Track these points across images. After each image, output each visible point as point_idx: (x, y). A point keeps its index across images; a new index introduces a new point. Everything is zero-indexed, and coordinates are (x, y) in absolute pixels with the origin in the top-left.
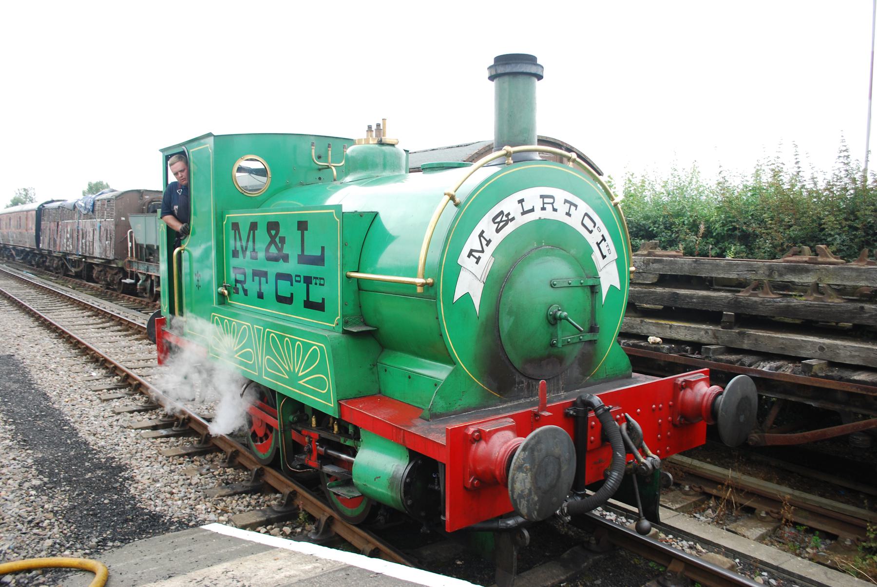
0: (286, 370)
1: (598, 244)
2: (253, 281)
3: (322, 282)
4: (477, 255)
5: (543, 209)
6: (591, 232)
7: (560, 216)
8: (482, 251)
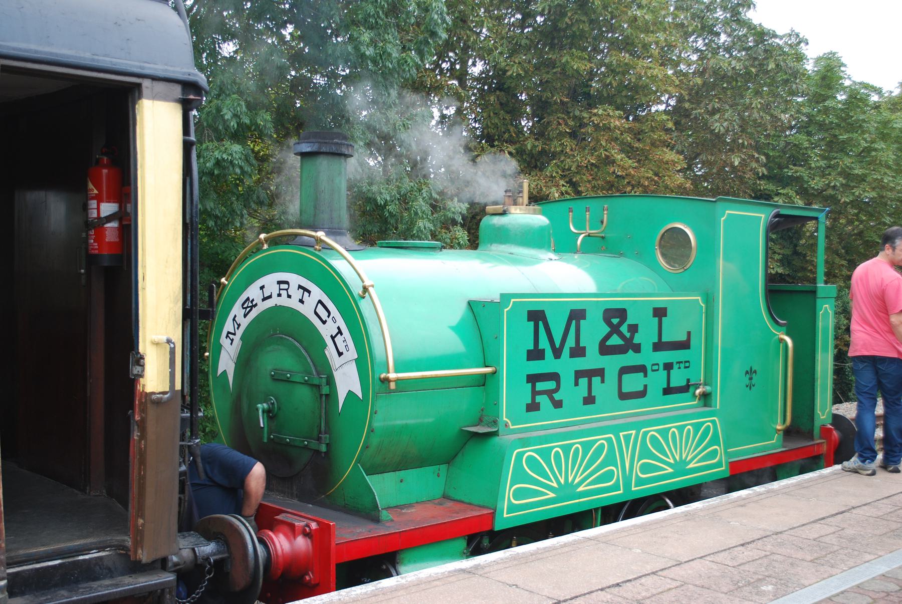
2: (576, 384)
3: (687, 364)
5: (279, 295)
7: (293, 304)
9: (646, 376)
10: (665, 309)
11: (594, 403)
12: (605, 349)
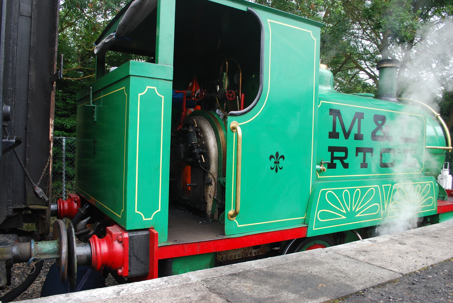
2: (357, 155)
10: (362, 114)
11: (335, 168)
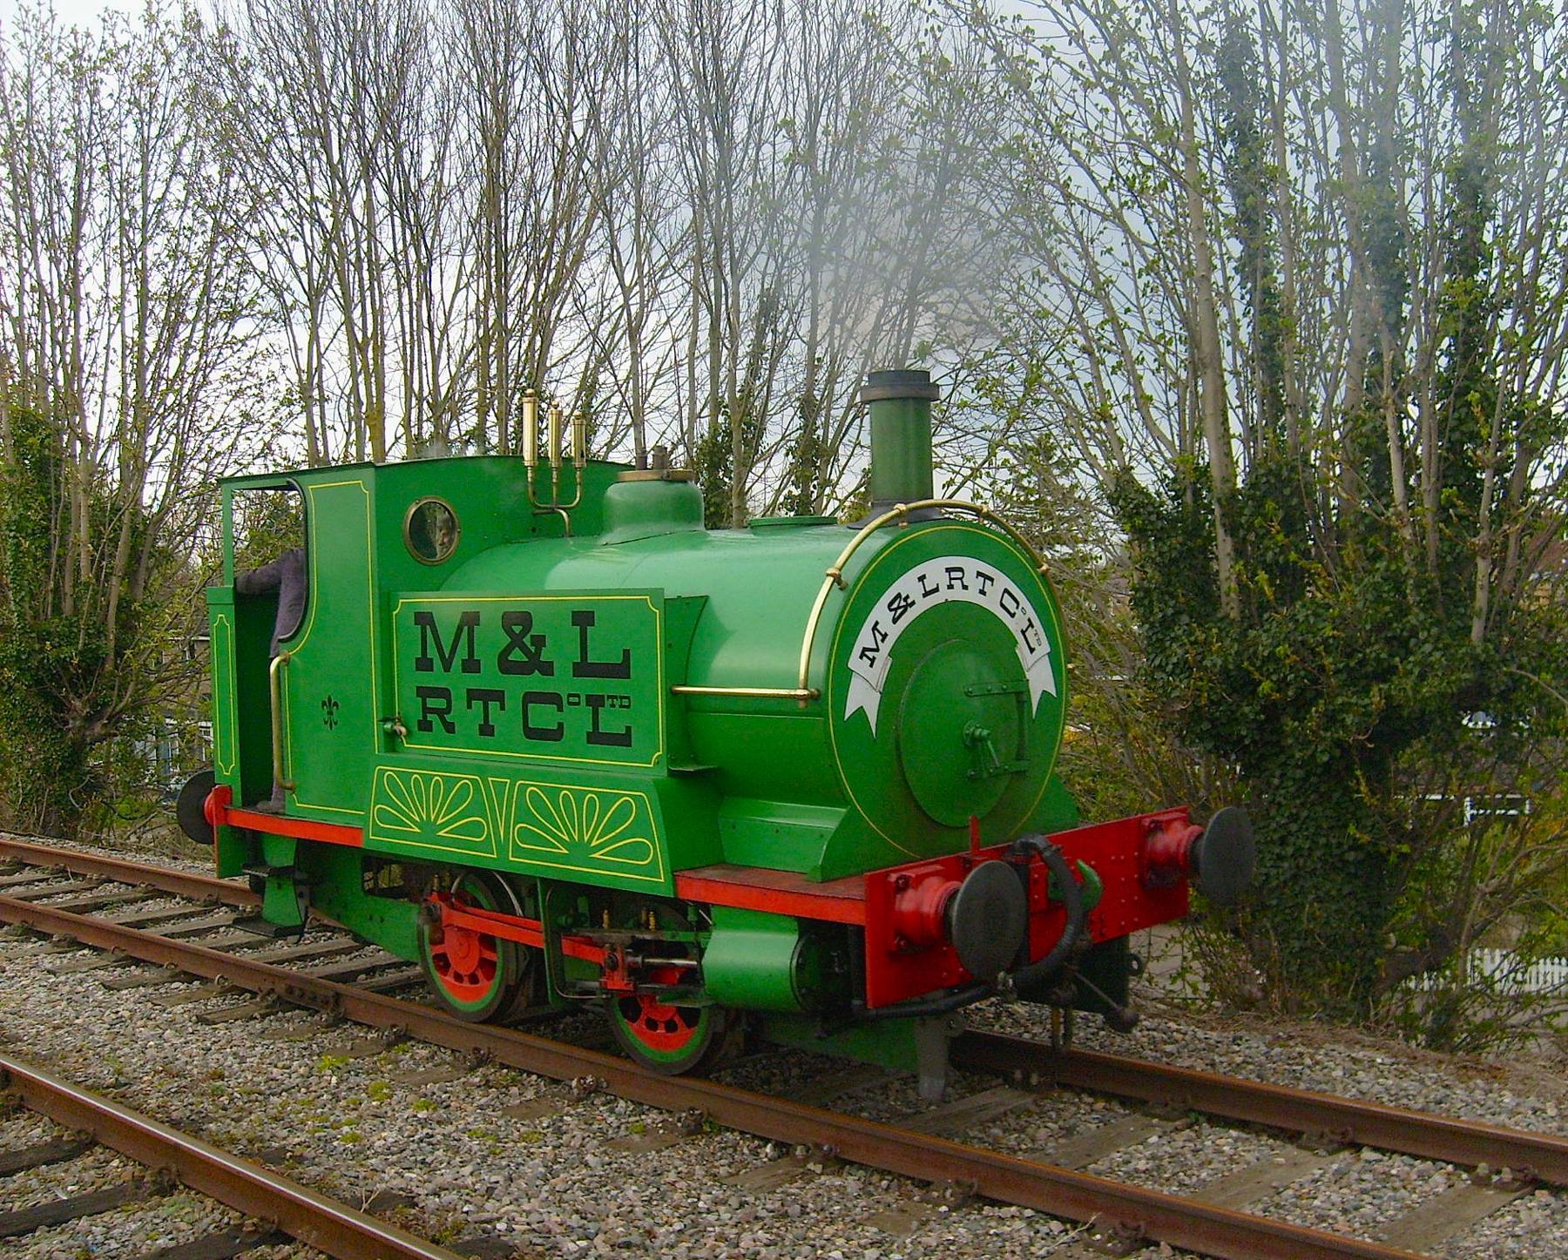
0: (561, 840)
1: (1023, 632)
2: (469, 706)
3: (625, 702)
4: (870, 654)
5: (951, 587)
6: (1013, 615)
7: (972, 596)
8: (877, 650)
9: (560, 709)
12: (506, 666)
